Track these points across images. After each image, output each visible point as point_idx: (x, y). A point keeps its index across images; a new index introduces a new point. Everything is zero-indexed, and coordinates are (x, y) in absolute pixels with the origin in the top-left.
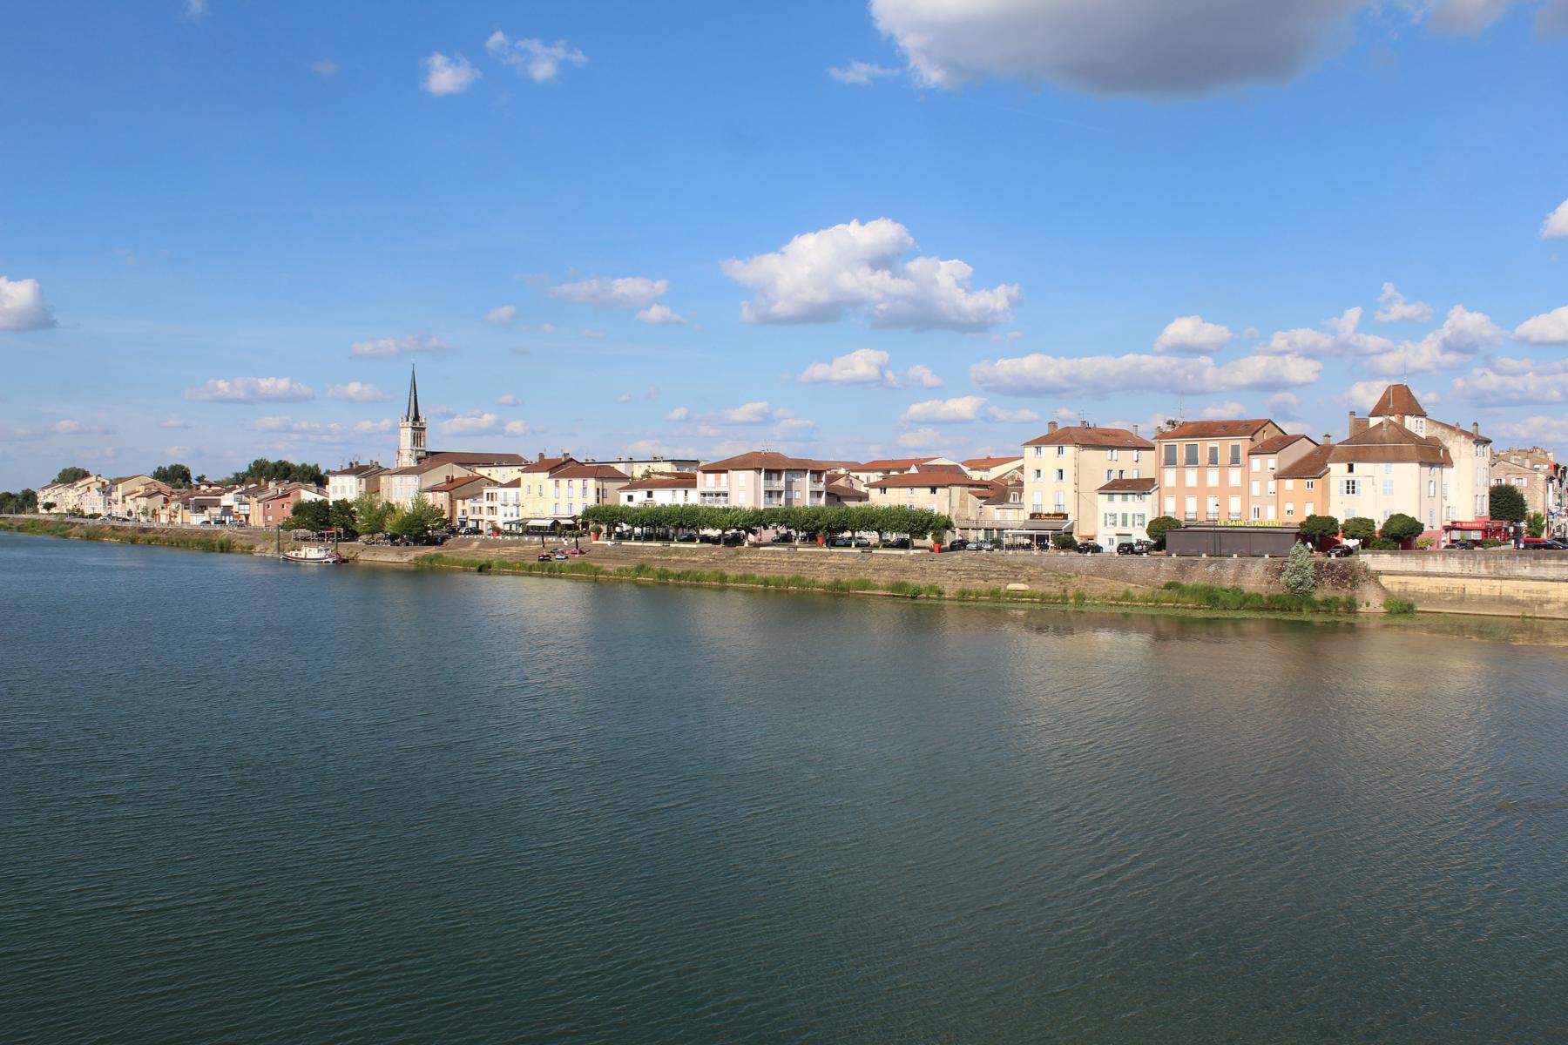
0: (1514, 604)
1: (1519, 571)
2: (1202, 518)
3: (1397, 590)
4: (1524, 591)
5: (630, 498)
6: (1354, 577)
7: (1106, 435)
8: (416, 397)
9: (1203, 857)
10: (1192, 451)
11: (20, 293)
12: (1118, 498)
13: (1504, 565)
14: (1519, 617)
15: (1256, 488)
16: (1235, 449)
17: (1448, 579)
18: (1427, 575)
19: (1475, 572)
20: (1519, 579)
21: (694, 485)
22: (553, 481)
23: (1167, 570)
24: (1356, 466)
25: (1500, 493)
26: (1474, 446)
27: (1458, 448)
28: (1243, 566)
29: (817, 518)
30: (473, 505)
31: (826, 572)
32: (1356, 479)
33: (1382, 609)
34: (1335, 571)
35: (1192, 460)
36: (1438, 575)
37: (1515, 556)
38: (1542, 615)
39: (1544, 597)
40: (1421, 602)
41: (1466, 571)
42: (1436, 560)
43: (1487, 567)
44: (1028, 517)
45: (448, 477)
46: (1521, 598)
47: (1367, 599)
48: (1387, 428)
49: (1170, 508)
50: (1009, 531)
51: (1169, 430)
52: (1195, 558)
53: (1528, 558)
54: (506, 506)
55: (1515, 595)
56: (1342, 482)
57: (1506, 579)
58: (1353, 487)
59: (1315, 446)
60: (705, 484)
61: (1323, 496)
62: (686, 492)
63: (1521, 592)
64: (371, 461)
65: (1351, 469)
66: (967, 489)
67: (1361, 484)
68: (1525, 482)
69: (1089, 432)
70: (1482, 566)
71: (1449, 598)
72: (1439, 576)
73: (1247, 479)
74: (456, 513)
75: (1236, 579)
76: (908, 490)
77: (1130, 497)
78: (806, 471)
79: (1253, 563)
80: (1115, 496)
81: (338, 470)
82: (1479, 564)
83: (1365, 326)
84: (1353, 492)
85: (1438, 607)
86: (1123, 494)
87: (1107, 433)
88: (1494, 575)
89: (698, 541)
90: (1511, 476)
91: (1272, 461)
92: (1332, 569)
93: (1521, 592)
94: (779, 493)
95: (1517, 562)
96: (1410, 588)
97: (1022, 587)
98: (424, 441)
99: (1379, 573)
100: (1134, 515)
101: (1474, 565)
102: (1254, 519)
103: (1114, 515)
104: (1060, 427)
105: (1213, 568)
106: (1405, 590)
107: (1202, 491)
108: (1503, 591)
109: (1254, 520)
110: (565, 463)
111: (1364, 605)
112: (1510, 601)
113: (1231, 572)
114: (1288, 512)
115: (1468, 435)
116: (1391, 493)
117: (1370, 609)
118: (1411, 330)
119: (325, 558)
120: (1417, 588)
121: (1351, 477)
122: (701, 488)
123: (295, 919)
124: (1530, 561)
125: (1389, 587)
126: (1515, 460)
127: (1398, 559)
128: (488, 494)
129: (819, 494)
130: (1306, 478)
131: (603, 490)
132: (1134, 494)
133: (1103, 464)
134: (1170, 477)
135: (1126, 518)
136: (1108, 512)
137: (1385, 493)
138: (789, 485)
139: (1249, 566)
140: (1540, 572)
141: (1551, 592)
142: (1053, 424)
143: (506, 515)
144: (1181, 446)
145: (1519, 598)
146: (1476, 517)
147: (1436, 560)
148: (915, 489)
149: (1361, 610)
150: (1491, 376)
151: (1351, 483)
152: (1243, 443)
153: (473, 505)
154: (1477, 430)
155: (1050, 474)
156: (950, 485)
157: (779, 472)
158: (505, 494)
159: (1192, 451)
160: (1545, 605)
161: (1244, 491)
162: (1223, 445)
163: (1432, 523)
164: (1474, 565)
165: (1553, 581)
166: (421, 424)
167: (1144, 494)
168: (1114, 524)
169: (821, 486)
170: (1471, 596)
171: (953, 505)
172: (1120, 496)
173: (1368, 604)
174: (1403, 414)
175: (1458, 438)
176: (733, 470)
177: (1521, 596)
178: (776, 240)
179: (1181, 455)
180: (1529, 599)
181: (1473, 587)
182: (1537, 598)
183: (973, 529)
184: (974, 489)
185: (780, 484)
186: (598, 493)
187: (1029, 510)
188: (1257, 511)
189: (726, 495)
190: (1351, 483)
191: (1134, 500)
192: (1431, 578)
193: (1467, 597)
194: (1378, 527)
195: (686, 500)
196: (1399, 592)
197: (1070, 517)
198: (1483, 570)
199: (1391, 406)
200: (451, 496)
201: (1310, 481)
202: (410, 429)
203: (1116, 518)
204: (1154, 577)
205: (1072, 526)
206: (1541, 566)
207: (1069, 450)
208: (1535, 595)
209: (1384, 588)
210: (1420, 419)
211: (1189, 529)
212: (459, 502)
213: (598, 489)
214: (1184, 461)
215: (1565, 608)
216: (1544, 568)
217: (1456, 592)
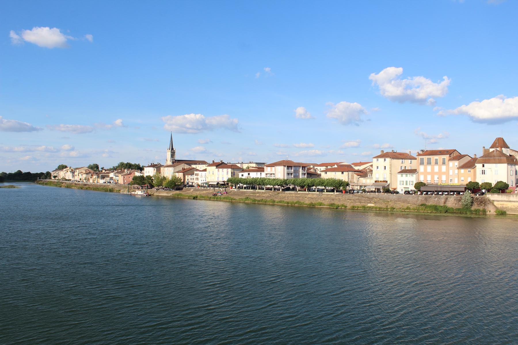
2: (432, 182)
5: (242, 175)
6: (485, 202)
8: (172, 141)
10: (429, 160)
15: (451, 172)
16: (444, 159)
18: (510, 201)
21: (263, 171)
22: (217, 169)
24: (485, 165)
33: (495, 213)
35: (429, 163)
36: (514, 202)
40: (508, 211)
44: (374, 182)
45: (183, 168)
62: (261, 173)
64: (158, 163)
65: (483, 166)
66: (354, 173)
73: (448, 169)
79: (450, 198)
81: (148, 166)
84: (484, 174)
87: (401, 154)
92: (477, 200)
94: (292, 174)
96: (504, 206)
98: (175, 156)
99: (494, 201)
100: (410, 181)
105: (436, 199)
106: (503, 207)
109: (450, 183)
111: (489, 212)
121: (483, 169)
122: (266, 172)
125: (497, 206)
136: (401, 180)
139: (449, 198)
143: (202, 181)
144: (425, 158)
147: (513, 197)
152: (447, 157)
155: (381, 168)
158: (202, 174)
161: (447, 173)
166: (174, 151)
173: (490, 211)
179: (425, 161)
187: (375, 180)
195: (261, 176)
197: (389, 182)
203: (403, 182)
205: (389, 185)
207: (388, 160)
209: (495, 206)
210: (507, 149)
214: (426, 164)
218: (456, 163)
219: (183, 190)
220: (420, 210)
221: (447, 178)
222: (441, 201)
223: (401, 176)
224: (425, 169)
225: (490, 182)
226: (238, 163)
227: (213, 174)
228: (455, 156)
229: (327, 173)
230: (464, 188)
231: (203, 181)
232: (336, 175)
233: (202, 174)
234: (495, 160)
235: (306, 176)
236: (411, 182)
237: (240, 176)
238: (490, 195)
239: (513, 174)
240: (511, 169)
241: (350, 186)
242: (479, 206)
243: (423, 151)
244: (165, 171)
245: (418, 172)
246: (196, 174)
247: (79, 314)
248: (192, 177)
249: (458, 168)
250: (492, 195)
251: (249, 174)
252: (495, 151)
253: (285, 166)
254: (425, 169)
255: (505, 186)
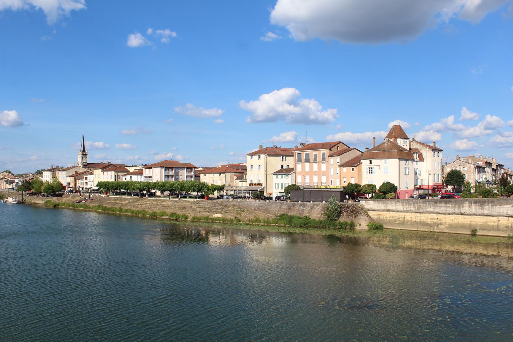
0: (426, 225)
1: (428, 209)
2: (311, 185)
3: (376, 218)
4: (430, 219)
5: (126, 179)
6: (356, 212)
7: (283, 151)
8: (84, 143)
9: (371, 314)
10: (307, 155)
11: (12, 115)
12: (280, 176)
13: (421, 206)
14: (428, 231)
15: (332, 172)
16: (324, 154)
17: (398, 213)
18: (388, 211)
19: (409, 210)
20: (428, 213)
21: (142, 174)
22: (102, 173)
23: (284, 208)
24: (372, 161)
25: (453, 173)
26: (433, 152)
27: (427, 153)
28: (313, 206)
29: (164, 186)
30: (81, 182)
31: (157, 208)
32: (373, 167)
33: (367, 227)
34: (349, 209)
35: (307, 160)
36: (393, 211)
37: (426, 202)
38: (438, 231)
39: (439, 221)
40: (386, 224)
41: (405, 209)
42: (392, 204)
43: (414, 207)
44: (248, 185)
45: (76, 172)
46: (429, 222)
47: (360, 222)
48: (387, 144)
49: (299, 181)
50: (237, 191)
51: (301, 147)
52: (296, 203)
53: (432, 203)
54: (90, 182)
55: (427, 221)
56: (367, 168)
57: (422, 213)
58: (372, 171)
59: (361, 153)
60: (146, 173)
61: (358, 175)
62: (141, 176)
63: (429, 219)
64: (56, 166)
65: (371, 163)
66: (234, 174)
67: (375, 169)
68: (466, 169)
69: (276, 149)
70: (412, 207)
71: (398, 222)
72: (393, 212)
73: (328, 168)
74: (77, 185)
75: (309, 213)
76: (212, 174)
77: (284, 176)
78: (185, 168)
79: (318, 205)
80: (279, 176)
81: (47, 169)
82: (410, 206)
83: (456, 122)
84: (372, 173)
85: (394, 226)
86: (281, 175)
87: (284, 150)
88: (417, 211)
89: (133, 195)
90: (461, 166)
91: (338, 159)
92: (348, 208)
93: (429, 219)
94: (172, 176)
95: (427, 204)
96: (381, 217)
97: (219, 215)
98: (87, 159)
99: (368, 210)
100: (285, 184)
101: (408, 206)
102: (331, 185)
103: (278, 184)
104: (264, 147)
105: (301, 207)
106: (379, 218)
107: (311, 173)
108: (421, 219)
109: (331, 186)
110: (108, 166)
111: (358, 225)
112: (425, 224)
113: (308, 209)
114: (345, 182)
115: (430, 147)
116: (387, 173)
117: (361, 227)
118: (472, 123)
119: (13, 202)
120: (385, 217)
121: (371, 166)
122: (145, 175)
123: (120, 316)
124: (433, 205)
125: (372, 216)
126: (463, 159)
127: (376, 203)
128: (85, 178)
129: (191, 177)
130: (351, 167)
131: (118, 176)
132: (285, 175)
133: (277, 163)
134: (299, 167)
135: (283, 185)
136: (276, 183)
137: (384, 173)
138: (177, 174)
139: (315, 206)
140: (437, 210)
141: (442, 220)
142: (261, 146)
143: (90, 186)
144: (303, 154)
145: (428, 222)
146: (434, 183)
147: (392, 204)
148: (214, 174)
149: (356, 228)
150: (500, 137)
151: (371, 168)
152: (327, 152)
153: (81, 182)
154: (435, 145)
155: (256, 167)
156: (225, 172)
157: (172, 168)
158: (90, 177)
159: (307, 155)
160: (440, 226)
161: (327, 173)
162: (319, 153)
163: (401, 187)
164: (408, 206)
165: (443, 214)
166: (86, 153)
167: (288, 175)
168: (279, 188)
169: (192, 174)
170: (407, 221)
171: (226, 180)
172: (280, 176)
173: (360, 225)
174: (396, 138)
175: (425, 149)
176: (154, 167)
177: (429, 221)
178: (256, 97)
179: (303, 157)
180: (432, 223)
181: (409, 217)
182: (436, 222)
183: (230, 190)
184: (237, 174)
185: (172, 173)
186: (116, 177)
187: (249, 182)
188: (332, 182)
189: (151, 177)
190: (371, 168)
191: (285, 178)
192: (391, 213)
193: (406, 221)
194: (378, 188)
195: (141, 179)
196: (377, 219)
197: (263, 185)
198: (413, 209)
199: (393, 135)
200: (75, 179)
201: (353, 168)
202: (81, 155)
203: (279, 185)
204: (278, 211)
205: (264, 189)
206: (438, 207)
207: (263, 157)
208: (435, 221)
209: (370, 217)
210: (405, 140)
211: (304, 190)
212: (78, 180)
213: (116, 176)
214: (313, 160)
215: (448, 228)
216: (439, 208)
217: (401, 219)
218: (336, 161)
219: (62, 197)
220: (270, 223)
221: (328, 178)
222: (306, 209)
223: (277, 178)
224: (303, 168)
225: (373, 184)
226: (142, 165)
227: (99, 178)
228: (341, 150)
229: (206, 174)
230: (339, 192)
231: (91, 185)
232: (214, 177)
233: (90, 177)
234: (384, 154)
235: (193, 179)
236: (277, 185)
237: (124, 180)
238: (364, 202)
239: (409, 173)
240: (406, 166)
241: (224, 190)
242: (348, 217)
243: (302, 144)
244: (60, 175)
245: (295, 172)
246: (85, 178)
247: (4, 319)
248: (82, 182)
249: (340, 166)
250: (366, 202)
251: (131, 178)
252: (386, 143)
253: (162, 167)
254: (303, 168)
255: (391, 188)
